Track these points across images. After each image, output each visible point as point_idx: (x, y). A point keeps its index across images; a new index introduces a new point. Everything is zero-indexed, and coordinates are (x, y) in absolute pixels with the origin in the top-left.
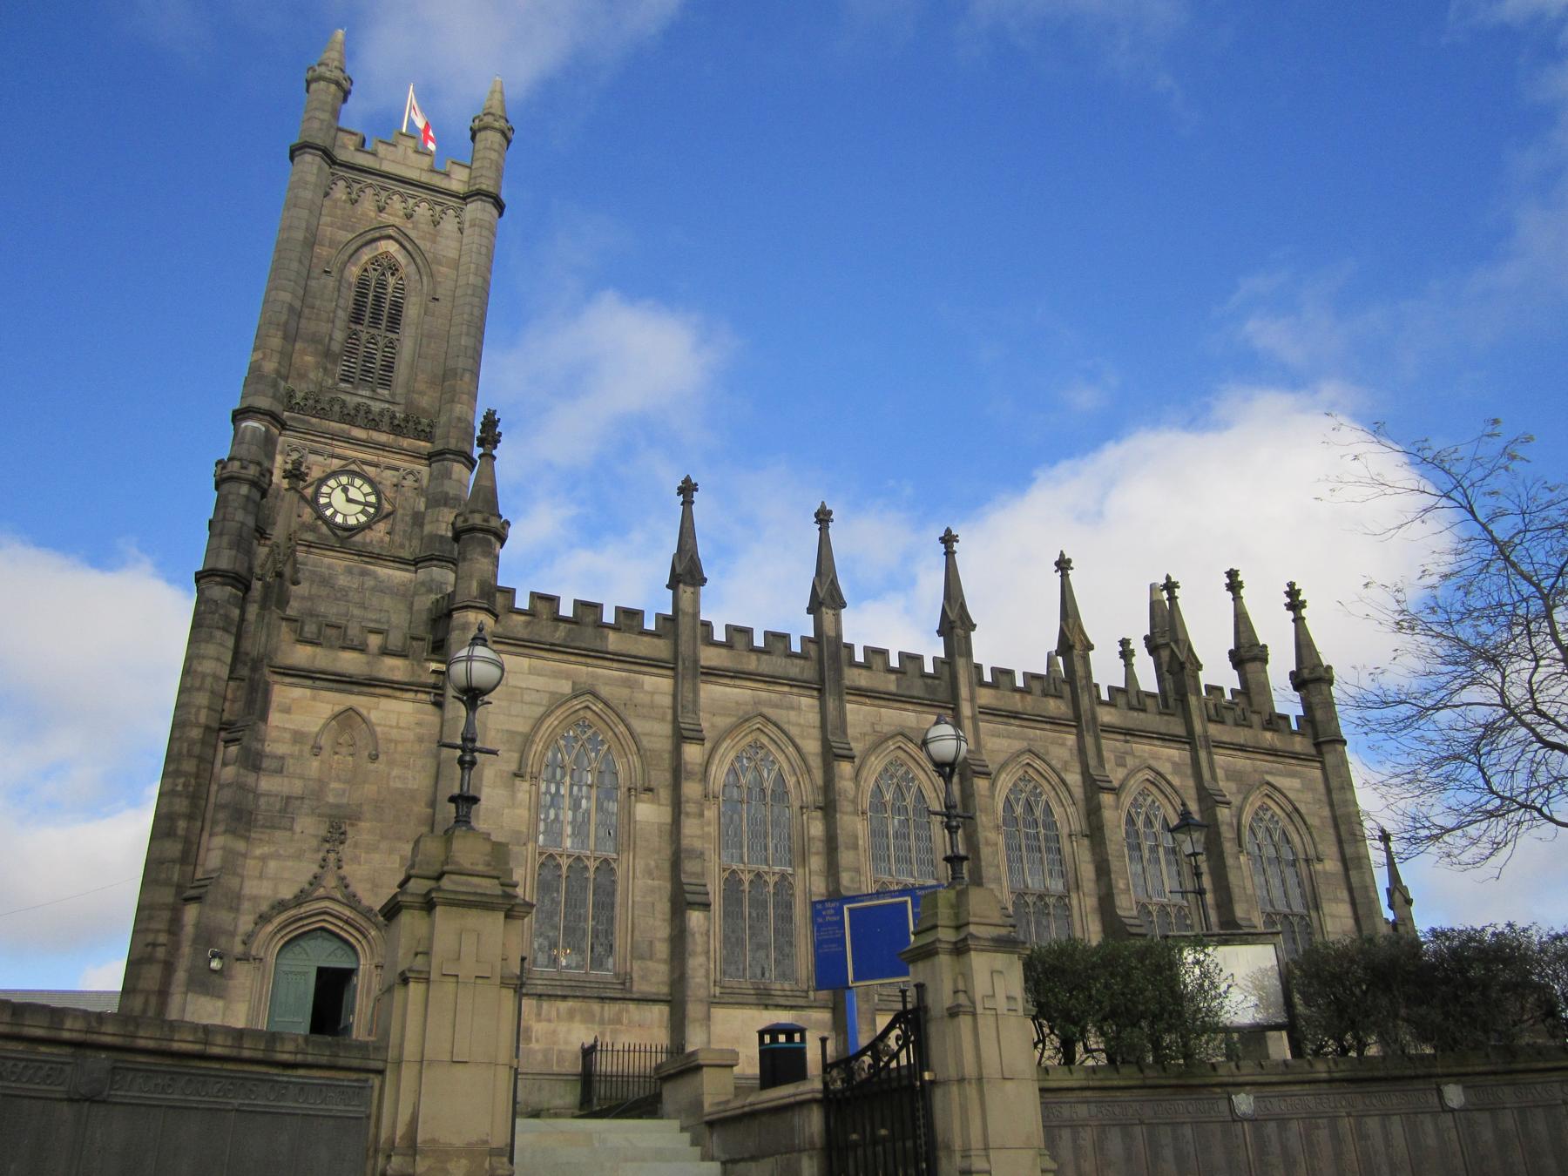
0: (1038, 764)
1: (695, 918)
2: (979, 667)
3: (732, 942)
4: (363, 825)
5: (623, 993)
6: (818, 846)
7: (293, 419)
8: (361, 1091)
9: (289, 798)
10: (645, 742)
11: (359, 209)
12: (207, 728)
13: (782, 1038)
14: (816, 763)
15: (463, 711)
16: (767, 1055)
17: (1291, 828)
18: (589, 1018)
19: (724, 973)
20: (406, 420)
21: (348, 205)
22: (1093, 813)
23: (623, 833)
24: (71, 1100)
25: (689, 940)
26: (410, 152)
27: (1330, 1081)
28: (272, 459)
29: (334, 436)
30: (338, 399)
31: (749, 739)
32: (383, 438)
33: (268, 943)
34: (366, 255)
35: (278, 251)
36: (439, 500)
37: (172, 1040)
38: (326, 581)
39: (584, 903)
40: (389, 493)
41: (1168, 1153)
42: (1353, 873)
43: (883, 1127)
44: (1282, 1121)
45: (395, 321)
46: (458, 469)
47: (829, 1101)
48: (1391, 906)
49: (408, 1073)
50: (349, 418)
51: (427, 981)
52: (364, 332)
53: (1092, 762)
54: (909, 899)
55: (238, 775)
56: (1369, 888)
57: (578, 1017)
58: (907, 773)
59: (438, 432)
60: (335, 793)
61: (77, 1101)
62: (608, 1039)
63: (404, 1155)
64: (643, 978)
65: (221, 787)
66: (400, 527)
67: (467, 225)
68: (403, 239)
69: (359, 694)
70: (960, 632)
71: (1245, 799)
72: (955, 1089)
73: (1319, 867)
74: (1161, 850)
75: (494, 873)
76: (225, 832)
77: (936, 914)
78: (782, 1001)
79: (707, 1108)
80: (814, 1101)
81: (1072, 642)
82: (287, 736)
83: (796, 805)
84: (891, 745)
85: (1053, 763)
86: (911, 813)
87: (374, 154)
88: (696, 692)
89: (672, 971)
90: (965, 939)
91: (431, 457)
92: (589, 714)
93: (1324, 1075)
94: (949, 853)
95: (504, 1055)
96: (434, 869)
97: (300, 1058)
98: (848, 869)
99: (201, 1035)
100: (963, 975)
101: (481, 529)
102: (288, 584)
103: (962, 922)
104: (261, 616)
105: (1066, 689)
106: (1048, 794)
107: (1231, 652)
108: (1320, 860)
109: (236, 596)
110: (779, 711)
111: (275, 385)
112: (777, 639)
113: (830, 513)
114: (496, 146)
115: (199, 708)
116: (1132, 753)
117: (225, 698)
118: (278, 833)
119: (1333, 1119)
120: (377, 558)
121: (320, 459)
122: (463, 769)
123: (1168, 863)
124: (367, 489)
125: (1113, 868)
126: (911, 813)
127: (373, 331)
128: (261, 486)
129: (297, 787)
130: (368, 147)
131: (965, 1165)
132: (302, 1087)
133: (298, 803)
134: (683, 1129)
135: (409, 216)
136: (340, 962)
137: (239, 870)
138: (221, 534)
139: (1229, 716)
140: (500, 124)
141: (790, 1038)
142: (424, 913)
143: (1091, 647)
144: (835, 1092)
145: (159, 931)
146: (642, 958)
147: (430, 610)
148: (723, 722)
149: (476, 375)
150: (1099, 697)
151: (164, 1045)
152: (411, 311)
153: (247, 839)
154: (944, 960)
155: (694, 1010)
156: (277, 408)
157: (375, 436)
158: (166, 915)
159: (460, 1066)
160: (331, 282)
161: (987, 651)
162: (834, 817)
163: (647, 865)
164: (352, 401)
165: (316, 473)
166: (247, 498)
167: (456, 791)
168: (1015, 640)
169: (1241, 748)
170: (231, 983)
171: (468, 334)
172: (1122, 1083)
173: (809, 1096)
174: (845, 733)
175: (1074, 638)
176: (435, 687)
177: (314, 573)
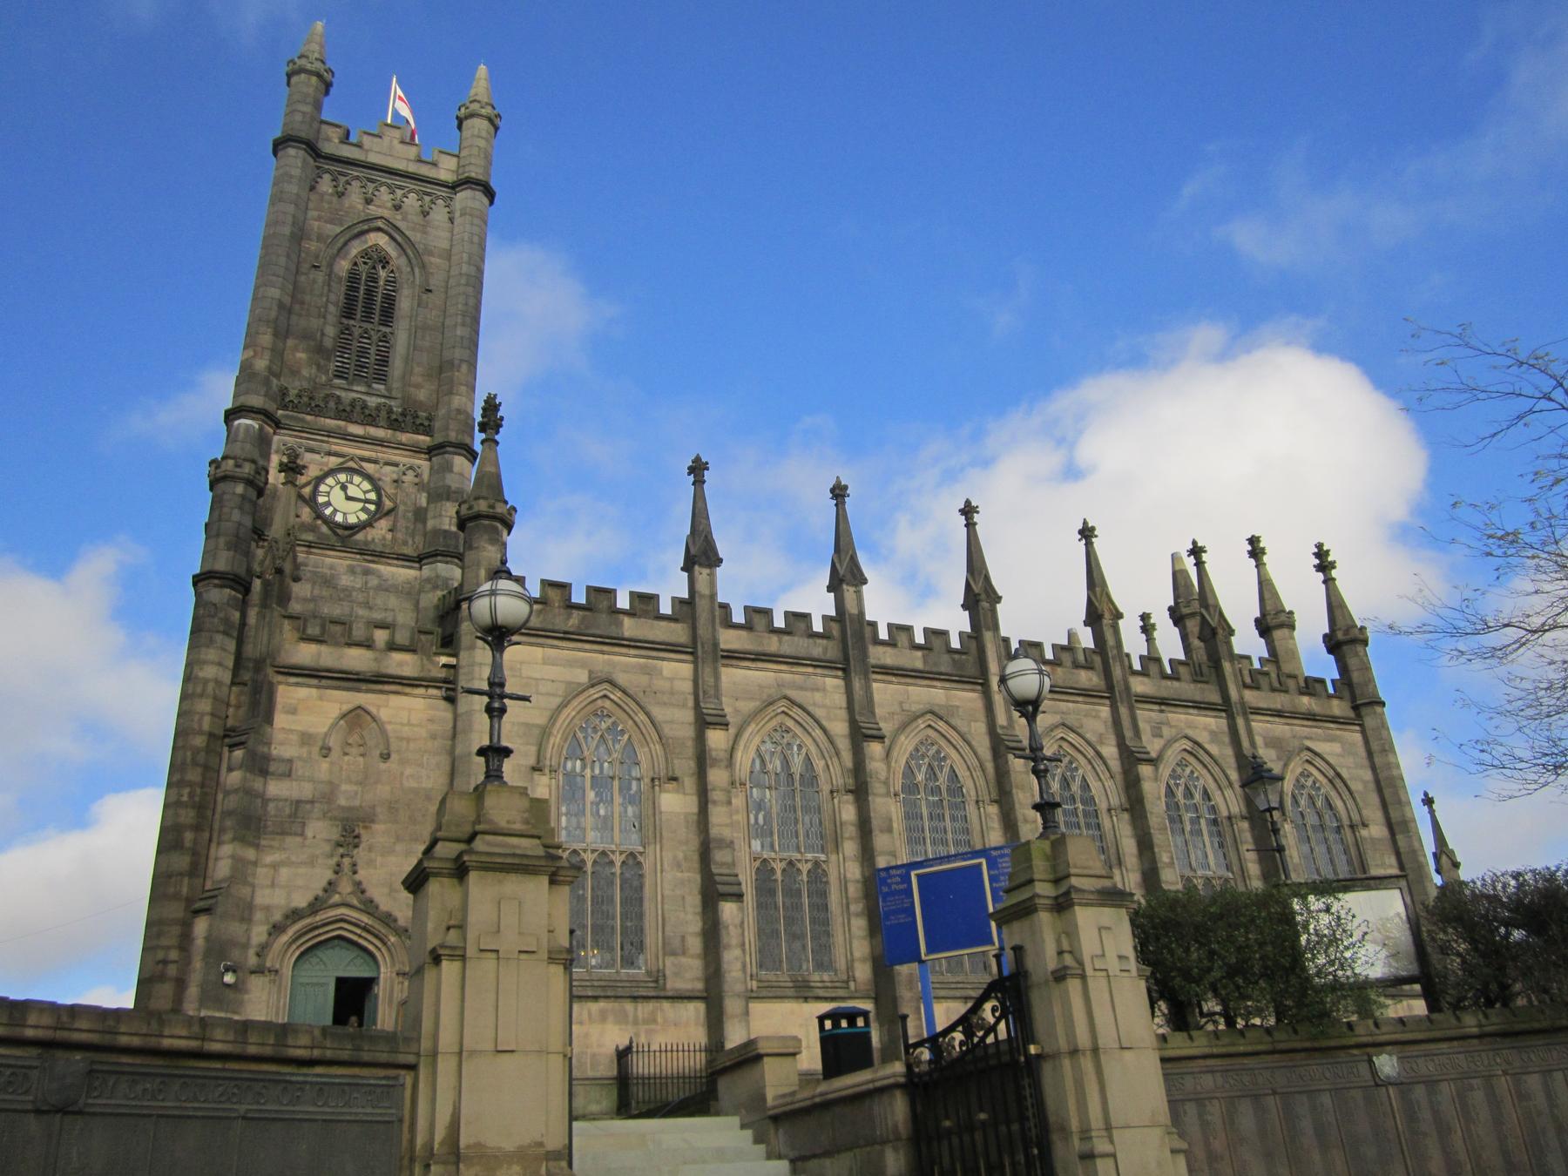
0: (1071, 737)
1: (728, 910)
2: (1006, 641)
3: (767, 934)
4: (377, 827)
5: (656, 991)
6: (851, 831)
7: (287, 417)
8: (390, 1090)
9: (298, 802)
10: (667, 730)
11: (346, 202)
12: (211, 735)
13: (844, 1024)
14: (844, 745)
15: (489, 653)
16: (827, 1041)
17: (1333, 794)
18: (622, 1019)
19: (761, 966)
20: (403, 414)
21: (335, 199)
22: (1132, 785)
23: (649, 825)
24: (38, 1112)
25: (723, 932)
26: (396, 142)
27: (1480, 1037)
28: (267, 457)
29: (330, 433)
30: (333, 395)
31: (774, 723)
32: (380, 433)
33: (283, 954)
34: (355, 249)
35: (265, 247)
36: (440, 494)
37: (162, 1036)
38: (328, 582)
39: (612, 900)
40: (389, 489)
41: (1306, 1125)
42: (1399, 837)
43: (982, 1110)
44: (1431, 1084)
45: (388, 315)
46: (459, 462)
47: (914, 1085)
48: (1438, 871)
49: (446, 1066)
50: (345, 413)
51: (463, 958)
52: (356, 326)
53: (1128, 734)
54: (984, 861)
55: (244, 779)
56: (1416, 853)
57: (611, 1018)
58: (938, 752)
59: (437, 425)
60: (347, 795)
61: (44, 1112)
62: (643, 1040)
63: (444, 1163)
64: (676, 974)
65: (227, 793)
66: (402, 523)
67: (457, 214)
68: (392, 231)
69: (367, 691)
70: (985, 604)
71: (1286, 765)
72: (1066, 1063)
73: (1364, 833)
74: (1203, 821)
75: (535, 832)
76: (234, 839)
77: (1031, 867)
78: (821, 993)
79: (770, 1101)
80: (897, 1086)
81: (1100, 612)
82: (294, 737)
83: (826, 788)
84: (921, 723)
85: (1088, 736)
86: (945, 793)
87: (359, 146)
88: (717, 677)
89: (707, 966)
90: (1067, 893)
91: (431, 451)
92: (607, 704)
93: (1475, 1030)
94: (1037, 799)
95: (556, 1043)
96: (467, 830)
97: (316, 1053)
98: (882, 853)
99: (196, 1029)
100: (1068, 934)
101: (487, 517)
102: (288, 580)
103: (1060, 875)
104: (261, 616)
105: (1097, 659)
106: (1084, 769)
107: (1257, 620)
108: (1365, 825)
109: (235, 598)
110: (802, 693)
111: (267, 382)
112: (798, 620)
113: (846, 487)
114: (484, 134)
115: (202, 715)
116: (1168, 724)
117: (228, 705)
118: (289, 839)
119: (1488, 1078)
120: (380, 556)
121: (317, 457)
122: (491, 717)
123: (1211, 835)
124: (366, 486)
125: (1156, 841)
126: (945, 793)
127: (365, 325)
128: (257, 486)
129: (304, 790)
130: (353, 139)
131: (1086, 1148)
132: (321, 1088)
133: (308, 806)
134: (743, 1127)
135: (397, 208)
136: (356, 969)
137: (250, 879)
138: (218, 535)
139: (1263, 681)
140: (487, 111)
141: (852, 1023)
142: (455, 881)
143: (1119, 616)
144: (920, 1075)
145: (168, 948)
146: (674, 954)
147: (437, 607)
148: (747, 706)
149: (473, 365)
150: (1131, 667)
151: (152, 1042)
152: (404, 304)
153: (257, 846)
154: (1044, 917)
155: (732, 1005)
156: (271, 406)
157: (372, 431)
158: (176, 930)
159: (507, 1056)
160: (320, 277)
161: (1014, 622)
162: (866, 800)
163: (675, 857)
164: (347, 396)
165: (313, 472)
166: (243, 497)
167: (486, 742)
168: (1042, 609)
169: (1279, 714)
170: (246, 997)
171: (463, 325)
172: (1249, 1049)
173: (891, 1081)
174: (873, 713)
175: (1103, 607)
176: (445, 681)
177: (315, 573)
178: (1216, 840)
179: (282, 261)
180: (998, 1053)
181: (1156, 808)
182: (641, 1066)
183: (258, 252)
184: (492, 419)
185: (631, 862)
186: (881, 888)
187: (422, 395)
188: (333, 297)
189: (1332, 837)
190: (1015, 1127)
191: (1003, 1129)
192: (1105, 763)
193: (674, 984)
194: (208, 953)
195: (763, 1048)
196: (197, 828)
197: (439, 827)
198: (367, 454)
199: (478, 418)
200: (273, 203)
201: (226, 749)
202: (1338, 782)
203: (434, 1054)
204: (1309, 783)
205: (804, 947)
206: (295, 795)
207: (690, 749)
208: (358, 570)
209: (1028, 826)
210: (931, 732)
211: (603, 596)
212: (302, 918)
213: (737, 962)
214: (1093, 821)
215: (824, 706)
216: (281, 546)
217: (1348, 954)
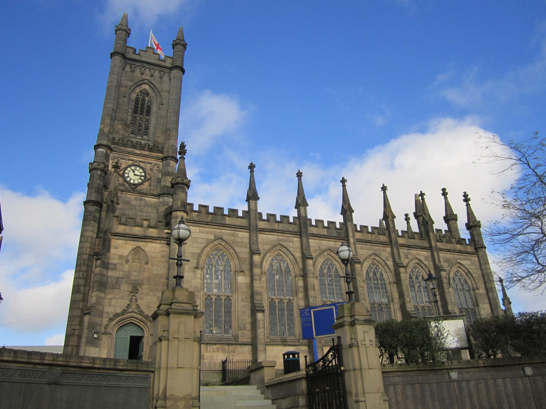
0: (377, 258)
1: (260, 315)
2: (355, 225)
3: (272, 323)
5: (235, 342)
6: (301, 289)
8: (147, 378)
9: (118, 278)
11: (135, 74)
12: (90, 255)
13: (291, 356)
14: (299, 260)
17: (467, 278)
18: (224, 351)
19: (270, 334)
20: (154, 146)
21: (131, 73)
22: (397, 275)
23: (233, 286)
24: (48, 384)
25: (258, 323)
26: (151, 53)
28: (108, 161)
29: (129, 153)
31: (276, 253)
32: (146, 153)
33: (113, 328)
34: (138, 90)
36: (166, 174)
38: (128, 203)
39: (221, 312)
40: (149, 172)
41: (428, 393)
42: (490, 293)
44: (468, 381)
45: (148, 113)
46: (172, 163)
47: (308, 378)
48: (504, 305)
49: (163, 372)
50: (134, 146)
51: (168, 340)
52: (138, 116)
53: (397, 257)
55: (101, 271)
57: (220, 351)
58: (332, 263)
59: (165, 150)
60: (134, 276)
62: (231, 358)
64: (242, 337)
65: (95, 275)
66: (153, 184)
67: (172, 78)
68: (150, 84)
69: (141, 241)
70: (348, 213)
71: (451, 268)
72: (352, 373)
73: (478, 291)
74: (422, 287)
75: (191, 302)
76: (97, 290)
77: (343, 312)
78: (291, 343)
79: (266, 381)
80: (303, 378)
82: (117, 257)
83: (293, 275)
84: (326, 253)
85: (383, 258)
87: (139, 55)
88: (257, 237)
89: (252, 334)
90: (354, 321)
91: (163, 159)
92: (220, 246)
93: (482, 365)
94: (347, 290)
95: (196, 365)
96: (170, 301)
97: (125, 368)
98: (312, 297)
99: (92, 361)
101: (181, 184)
102: (115, 204)
103: (353, 314)
104: (106, 216)
105: (387, 232)
106: (381, 269)
108: (478, 289)
111: (108, 136)
112: (285, 218)
114: (181, 50)
115: (87, 248)
116: (410, 254)
117: (95, 245)
119: (486, 380)
120: (145, 194)
122: (178, 267)
123: (424, 292)
127: (141, 116)
128: (105, 171)
129: (121, 274)
130: (137, 52)
132: (127, 378)
133: (121, 280)
134: (258, 389)
135: (152, 76)
136: (138, 334)
137: (102, 303)
138: (92, 188)
139: (444, 240)
141: (294, 356)
143: (394, 217)
144: (310, 375)
145: (75, 325)
148: (267, 247)
150: (398, 234)
151: (79, 364)
152: (154, 109)
153: (104, 292)
154: (347, 328)
155: (260, 347)
156: (109, 144)
157: (143, 152)
158: (78, 319)
160: (126, 100)
161: (358, 219)
165: (123, 166)
166: (100, 175)
167: (176, 274)
168: (368, 215)
169: (449, 251)
171: (174, 116)
172: (411, 369)
174: (309, 250)
176: (167, 238)
177: (124, 200)
178: (426, 293)
179: (113, 94)
180: (333, 369)
181: (405, 282)
182: (230, 367)
183: (105, 92)
184: (183, 151)
185: (227, 298)
186: (305, 312)
187: (160, 140)
188: (130, 107)
189: (467, 293)
190: (337, 392)
191: (333, 392)
192: (388, 267)
193: (241, 340)
194: (89, 328)
195: (264, 364)
196: (85, 286)
197: (162, 301)
198: (141, 160)
199: (178, 150)
200: (110, 75)
201: (95, 260)
202: (469, 274)
203: (160, 368)
204: (459, 274)
205: (285, 328)
206: (117, 276)
207: (248, 262)
208: (138, 199)
209: (361, 289)
210: (329, 256)
211: (219, 210)
212: (119, 316)
213: (261, 333)
214: (384, 287)
215: (293, 247)
216: (113, 193)
217: (443, 341)
